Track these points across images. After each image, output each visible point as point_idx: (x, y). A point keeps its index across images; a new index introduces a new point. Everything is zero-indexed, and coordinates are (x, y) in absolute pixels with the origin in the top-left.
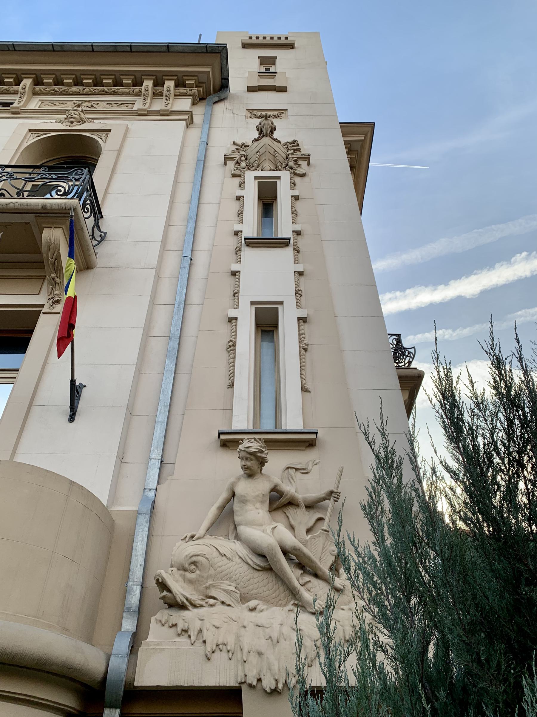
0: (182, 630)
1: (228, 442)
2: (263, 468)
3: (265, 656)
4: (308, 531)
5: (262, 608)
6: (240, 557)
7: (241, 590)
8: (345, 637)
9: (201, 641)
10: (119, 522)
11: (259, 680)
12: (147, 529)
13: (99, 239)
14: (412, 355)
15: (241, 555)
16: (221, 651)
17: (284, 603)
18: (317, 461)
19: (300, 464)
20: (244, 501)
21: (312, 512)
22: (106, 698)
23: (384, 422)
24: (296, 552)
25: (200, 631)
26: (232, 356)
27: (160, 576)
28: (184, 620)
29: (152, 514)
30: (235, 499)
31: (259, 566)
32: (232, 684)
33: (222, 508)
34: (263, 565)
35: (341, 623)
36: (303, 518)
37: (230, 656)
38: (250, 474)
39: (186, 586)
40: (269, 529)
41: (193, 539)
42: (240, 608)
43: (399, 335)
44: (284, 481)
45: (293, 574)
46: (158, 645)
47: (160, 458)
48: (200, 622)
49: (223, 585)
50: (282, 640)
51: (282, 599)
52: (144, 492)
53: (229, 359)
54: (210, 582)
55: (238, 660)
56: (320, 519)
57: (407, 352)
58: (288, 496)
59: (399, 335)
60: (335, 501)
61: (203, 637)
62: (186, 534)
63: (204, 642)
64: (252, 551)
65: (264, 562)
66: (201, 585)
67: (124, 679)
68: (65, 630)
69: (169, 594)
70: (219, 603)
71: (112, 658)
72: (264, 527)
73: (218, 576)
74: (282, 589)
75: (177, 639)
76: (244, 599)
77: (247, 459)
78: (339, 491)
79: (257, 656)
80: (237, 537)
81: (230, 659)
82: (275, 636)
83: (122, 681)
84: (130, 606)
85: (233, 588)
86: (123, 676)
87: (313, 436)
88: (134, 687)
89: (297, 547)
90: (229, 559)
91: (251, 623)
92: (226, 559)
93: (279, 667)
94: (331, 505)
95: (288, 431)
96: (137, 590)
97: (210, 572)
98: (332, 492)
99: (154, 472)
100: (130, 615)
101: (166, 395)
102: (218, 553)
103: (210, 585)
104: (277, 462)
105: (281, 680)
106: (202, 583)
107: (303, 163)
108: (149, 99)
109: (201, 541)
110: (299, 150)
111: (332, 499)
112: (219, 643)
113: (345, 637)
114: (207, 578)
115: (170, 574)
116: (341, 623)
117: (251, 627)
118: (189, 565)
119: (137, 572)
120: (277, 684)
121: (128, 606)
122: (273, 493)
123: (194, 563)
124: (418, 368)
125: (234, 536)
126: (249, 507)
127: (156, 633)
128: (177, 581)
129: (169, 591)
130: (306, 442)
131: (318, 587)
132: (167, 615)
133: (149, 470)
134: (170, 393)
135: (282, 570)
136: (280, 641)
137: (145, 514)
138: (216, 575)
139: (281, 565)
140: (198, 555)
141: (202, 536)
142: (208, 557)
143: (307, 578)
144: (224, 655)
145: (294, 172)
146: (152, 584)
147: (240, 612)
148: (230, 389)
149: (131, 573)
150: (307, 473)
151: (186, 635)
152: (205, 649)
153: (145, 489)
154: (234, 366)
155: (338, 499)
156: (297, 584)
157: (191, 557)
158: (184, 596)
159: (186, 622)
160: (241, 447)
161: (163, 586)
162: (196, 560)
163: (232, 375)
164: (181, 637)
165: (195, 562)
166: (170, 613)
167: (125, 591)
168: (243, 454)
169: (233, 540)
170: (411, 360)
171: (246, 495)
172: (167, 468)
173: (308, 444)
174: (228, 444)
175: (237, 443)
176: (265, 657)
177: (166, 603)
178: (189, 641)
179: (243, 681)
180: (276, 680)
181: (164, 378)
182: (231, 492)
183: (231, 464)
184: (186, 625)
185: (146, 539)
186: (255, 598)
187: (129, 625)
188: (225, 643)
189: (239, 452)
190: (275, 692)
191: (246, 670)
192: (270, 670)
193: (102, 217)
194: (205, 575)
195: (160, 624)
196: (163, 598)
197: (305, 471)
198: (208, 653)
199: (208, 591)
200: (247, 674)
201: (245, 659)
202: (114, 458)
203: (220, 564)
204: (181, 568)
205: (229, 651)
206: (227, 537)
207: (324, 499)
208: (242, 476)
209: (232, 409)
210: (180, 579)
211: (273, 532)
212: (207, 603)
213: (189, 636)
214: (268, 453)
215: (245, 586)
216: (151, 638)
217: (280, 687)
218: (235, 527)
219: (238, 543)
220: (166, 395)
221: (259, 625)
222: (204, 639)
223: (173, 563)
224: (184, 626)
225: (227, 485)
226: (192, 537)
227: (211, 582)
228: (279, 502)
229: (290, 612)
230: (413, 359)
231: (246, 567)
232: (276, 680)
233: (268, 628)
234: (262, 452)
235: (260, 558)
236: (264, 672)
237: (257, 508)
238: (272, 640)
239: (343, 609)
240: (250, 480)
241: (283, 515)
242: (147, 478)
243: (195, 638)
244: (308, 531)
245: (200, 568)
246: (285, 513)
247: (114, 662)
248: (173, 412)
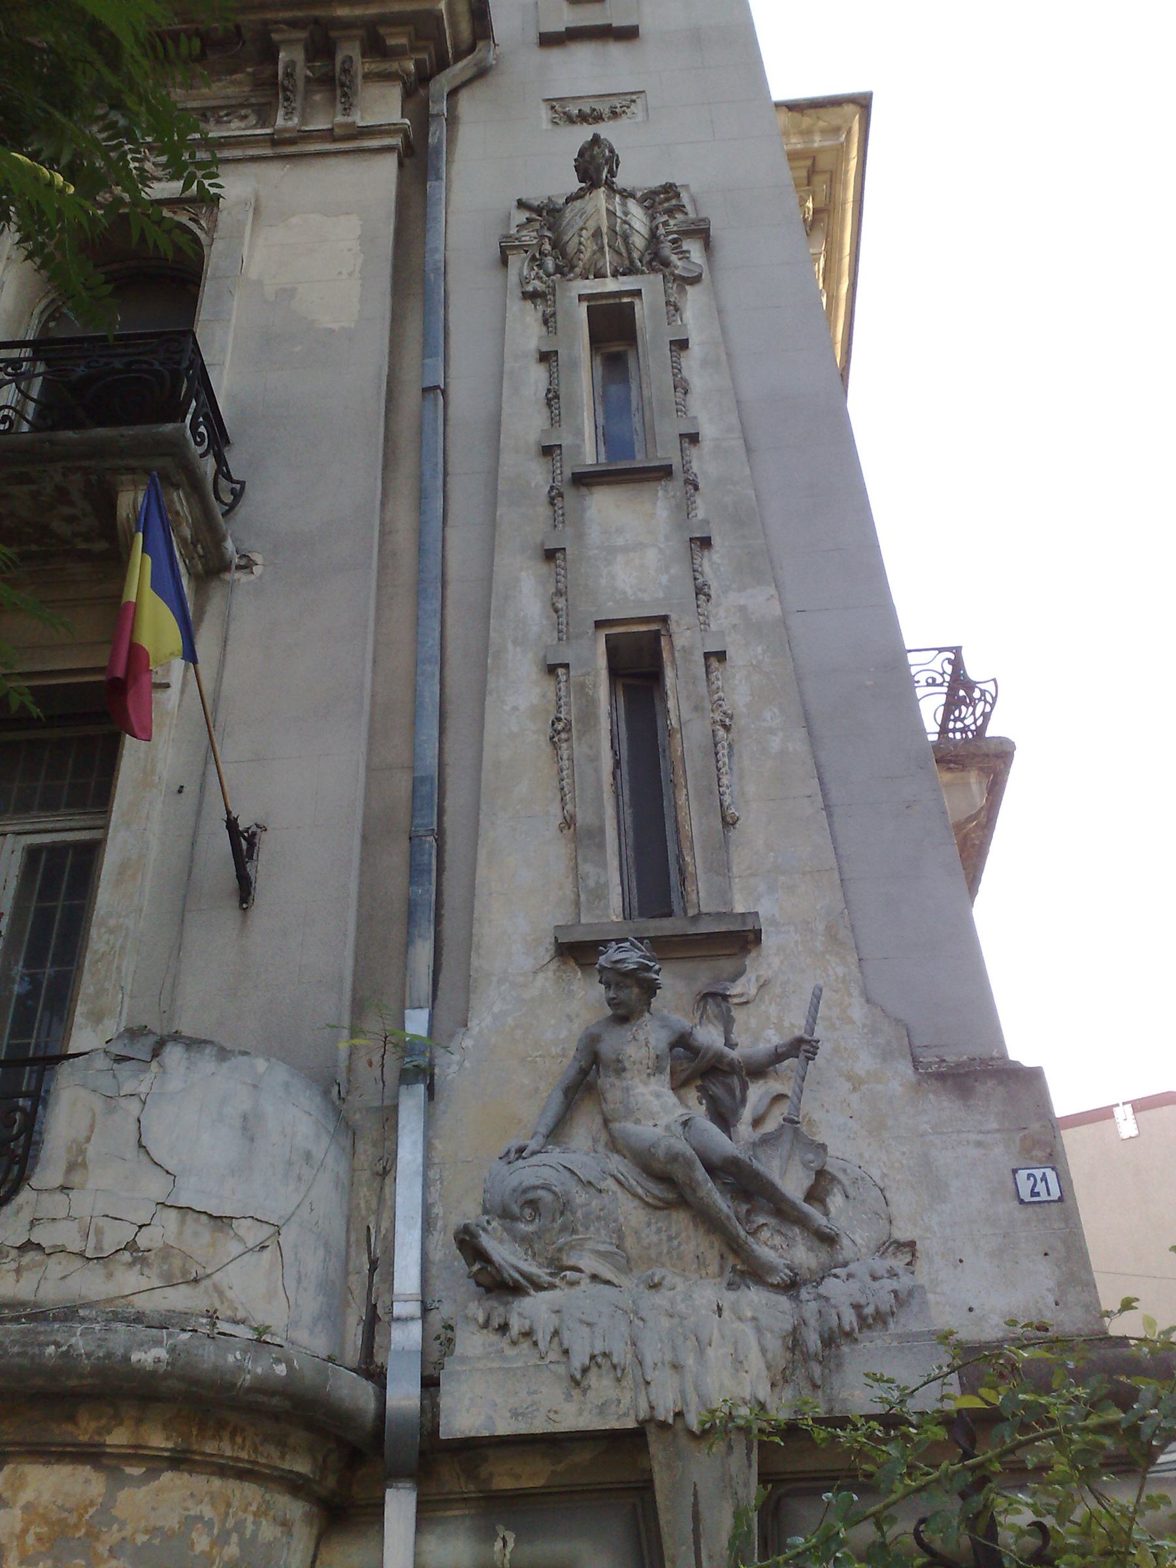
13: (228, 499)
14: (989, 698)
25: (556, 1333)
34: (670, 1196)
43: (957, 650)
58: (710, 1054)
59: (957, 650)
60: (809, 1059)
63: (566, 1352)
98: (800, 1041)
103: (566, 1244)
107: (693, 247)
108: (299, 99)
110: (681, 208)
111: (802, 1055)
127: (472, 1343)
128: (501, 1241)
145: (673, 274)
150: (747, 1003)
160: (602, 960)
170: (988, 709)
183: (587, 998)
193: (228, 442)
213: (535, 1344)
224: (523, 1326)
226: (521, 1150)
230: (992, 706)
234: (649, 969)
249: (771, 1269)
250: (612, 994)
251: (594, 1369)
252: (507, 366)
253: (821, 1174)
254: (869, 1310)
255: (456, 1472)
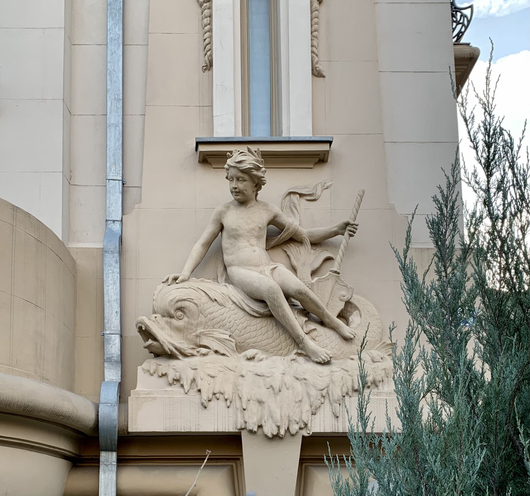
0: (174, 380)
1: (210, 156)
2: (259, 192)
3: (266, 405)
4: (314, 273)
5: (261, 357)
6: (234, 303)
7: (237, 338)
8: (353, 387)
9: (196, 390)
10: (81, 262)
11: (260, 427)
12: (118, 270)
14: (466, 23)
15: (235, 300)
16: (218, 399)
17: (285, 352)
18: (328, 184)
19: (306, 187)
20: (236, 236)
21: (319, 250)
22: (100, 441)
23: (492, 86)
24: (300, 297)
25: (194, 380)
26: (207, 12)
27: (142, 323)
28: (174, 369)
29: (121, 252)
30: (224, 233)
31: (257, 312)
32: (231, 430)
33: (208, 244)
34: (262, 311)
35: (350, 373)
36: (306, 257)
37: (228, 404)
38: (243, 201)
39: (173, 333)
40: (267, 270)
41: (177, 281)
42: (236, 357)
44: (284, 210)
45: (297, 321)
46: (149, 394)
47: (120, 178)
48: (193, 371)
49: (215, 333)
50: (284, 389)
51: (283, 348)
52: (106, 225)
53: (203, 19)
54: (200, 330)
55: (236, 408)
56: (328, 259)
57: (459, 14)
58: (290, 231)
60: (351, 236)
61: (197, 386)
62: (167, 276)
63: (199, 391)
64: (248, 295)
65: (264, 308)
66: (191, 333)
67: (117, 426)
68: (44, 379)
69: (155, 343)
70: (212, 352)
71: (101, 406)
72: (261, 268)
73: (209, 323)
74: (283, 337)
75: (170, 389)
76: (240, 348)
77: (238, 179)
78: (356, 223)
79: (257, 404)
80: (229, 280)
81: (228, 407)
82: (277, 385)
83: (115, 427)
84: (110, 356)
85: (227, 337)
86: (116, 423)
87: (324, 147)
88: (128, 433)
89: (303, 291)
90: (221, 305)
91: (249, 373)
92: (218, 305)
93: (281, 414)
94: (344, 241)
95: (292, 139)
96: (116, 340)
97: (199, 319)
98: (347, 224)
99: (115, 199)
100: (112, 365)
101: (115, 82)
102: (208, 299)
103: (201, 333)
104: (277, 184)
105: (283, 426)
106: (191, 331)
109: (185, 284)
111: (346, 233)
112: (215, 392)
113: (353, 387)
114: (197, 325)
115: (154, 321)
116: (350, 373)
117: (249, 377)
118: (175, 311)
119: (114, 320)
120: (279, 430)
121: (108, 356)
122: (271, 226)
123: (180, 309)
124: (473, 45)
125: (224, 278)
126: (243, 243)
128: (162, 329)
129: (155, 339)
130: (314, 156)
131: (324, 336)
132: (155, 365)
133: (108, 195)
134: (121, 79)
135: (284, 316)
136: (282, 391)
137: (112, 252)
138: (206, 323)
139: (283, 310)
140: (184, 300)
141: (186, 278)
142: (196, 302)
143: (312, 326)
144: (221, 403)
146: (133, 333)
147: (237, 361)
148: (207, 71)
149: (106, 321)
150: (315, 200)
151: (178, 385)
152: (201, 398)
153: (107, 220)
154: (210, 30)
155: (354, 233)
156: (301, 332)
157: (178, 301)
158: (172, 345)
159: (177, 372)
160: (229, 161)
161: (146, 333)
162: (183, 306)
163: (208, 47)
164: (173, 386)
165: (181, 307)
166: (158, 363)
167: (102, 341)
168: (233, 172)
169: (224, 284)
170: (463, 30)
171: (238, 228)
172: (132, 193)
173: (317, 160)
174: (209, 160)
175: (223, 157)
176: (266, 404)
177: (151, 353)
178: (181, 390)
179: (243, 427)
180: (278, 427)
181: (109, 52)
182: (219, 225)
184: (178, 374)
185: (119, 282)
186: (253, 347)
187: (112, 375)
188: (222, 392)
189: (227, 169)
190: (276, 437)
191: (246, 416)
192: (272, 417)
194: (194, 322)
195: (148, 374)
196: (147, 347)
197: (312, 198)
198: (204, 402)
199: (198, 339)
200: (247, 421)
201: (245, 408)
202: (59, 178)
203: (211, 310)
204: (166, 315)
205: (226, 400)
206: (216, 279)
207: (336, 234)
208: (231, 203)
209: (212, 106)
210: (167, 326)
211: (272, 274)
212: (198, 352)
213: (182, 386)
214: (265, 171)
215: (241, 334)
216: (139, 387)
217: (282, 432)
218: (225, 268)
219: (230, 287)
220: (115, 82)
221: (259, 374)
222: (199, 388)
223: (156, 309)
224: (175, 376)
225: (213, 216)
226: (175, 279)
227: (202, 330)
228: (279, 238)
229: (293, 361)
230: (466, 28)
231: (241, 313)
232: (278, 427)
233: (268, 377)
235: (259, 304)
236: (266, 419)
237: (252, 245)
238: (273, 389)
239: (352, 359)
240: (243, 208)
241: (283, 255)
242: (108, 205)
243: (189, 387)
244: (314, 273)
245: (188, 314)
246: (286, 252)
247: (103, 410)
248: (129, 111)
249: (315, 353)
250: (234, 185)
251: (214, 400)
252: (121, 32)
253: (348, 303)
254: (369, 379)
255: (138, 448)
